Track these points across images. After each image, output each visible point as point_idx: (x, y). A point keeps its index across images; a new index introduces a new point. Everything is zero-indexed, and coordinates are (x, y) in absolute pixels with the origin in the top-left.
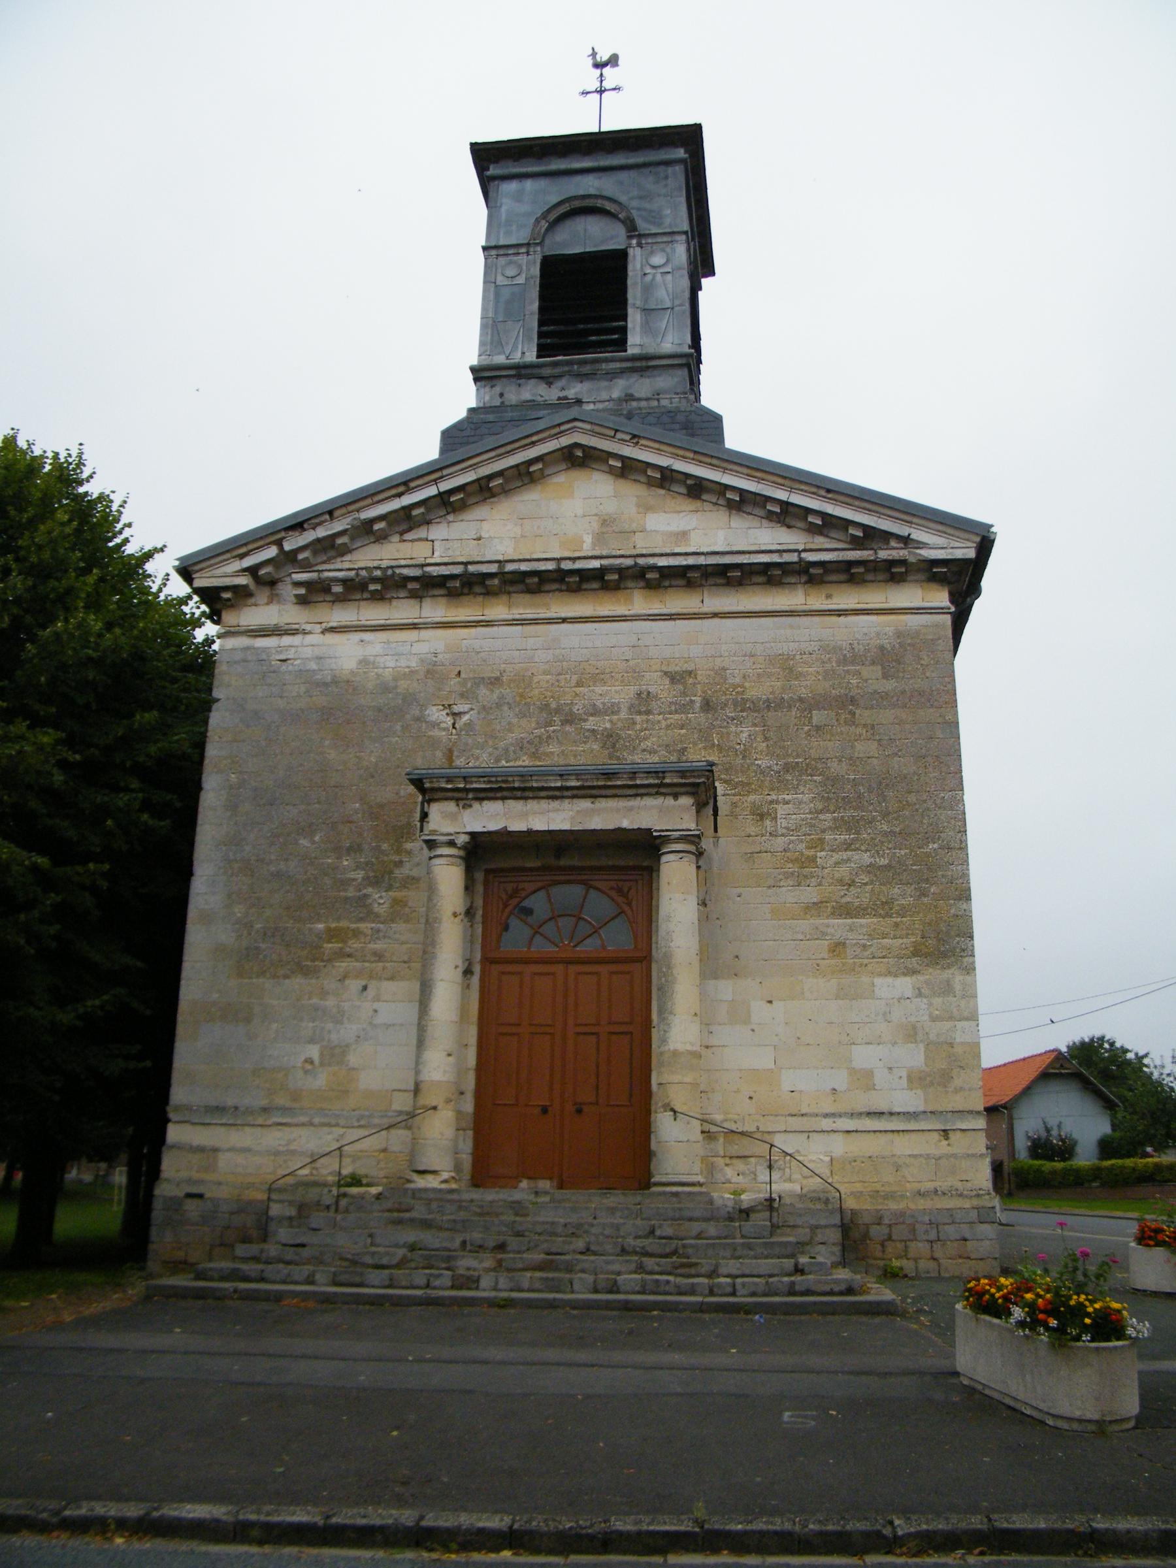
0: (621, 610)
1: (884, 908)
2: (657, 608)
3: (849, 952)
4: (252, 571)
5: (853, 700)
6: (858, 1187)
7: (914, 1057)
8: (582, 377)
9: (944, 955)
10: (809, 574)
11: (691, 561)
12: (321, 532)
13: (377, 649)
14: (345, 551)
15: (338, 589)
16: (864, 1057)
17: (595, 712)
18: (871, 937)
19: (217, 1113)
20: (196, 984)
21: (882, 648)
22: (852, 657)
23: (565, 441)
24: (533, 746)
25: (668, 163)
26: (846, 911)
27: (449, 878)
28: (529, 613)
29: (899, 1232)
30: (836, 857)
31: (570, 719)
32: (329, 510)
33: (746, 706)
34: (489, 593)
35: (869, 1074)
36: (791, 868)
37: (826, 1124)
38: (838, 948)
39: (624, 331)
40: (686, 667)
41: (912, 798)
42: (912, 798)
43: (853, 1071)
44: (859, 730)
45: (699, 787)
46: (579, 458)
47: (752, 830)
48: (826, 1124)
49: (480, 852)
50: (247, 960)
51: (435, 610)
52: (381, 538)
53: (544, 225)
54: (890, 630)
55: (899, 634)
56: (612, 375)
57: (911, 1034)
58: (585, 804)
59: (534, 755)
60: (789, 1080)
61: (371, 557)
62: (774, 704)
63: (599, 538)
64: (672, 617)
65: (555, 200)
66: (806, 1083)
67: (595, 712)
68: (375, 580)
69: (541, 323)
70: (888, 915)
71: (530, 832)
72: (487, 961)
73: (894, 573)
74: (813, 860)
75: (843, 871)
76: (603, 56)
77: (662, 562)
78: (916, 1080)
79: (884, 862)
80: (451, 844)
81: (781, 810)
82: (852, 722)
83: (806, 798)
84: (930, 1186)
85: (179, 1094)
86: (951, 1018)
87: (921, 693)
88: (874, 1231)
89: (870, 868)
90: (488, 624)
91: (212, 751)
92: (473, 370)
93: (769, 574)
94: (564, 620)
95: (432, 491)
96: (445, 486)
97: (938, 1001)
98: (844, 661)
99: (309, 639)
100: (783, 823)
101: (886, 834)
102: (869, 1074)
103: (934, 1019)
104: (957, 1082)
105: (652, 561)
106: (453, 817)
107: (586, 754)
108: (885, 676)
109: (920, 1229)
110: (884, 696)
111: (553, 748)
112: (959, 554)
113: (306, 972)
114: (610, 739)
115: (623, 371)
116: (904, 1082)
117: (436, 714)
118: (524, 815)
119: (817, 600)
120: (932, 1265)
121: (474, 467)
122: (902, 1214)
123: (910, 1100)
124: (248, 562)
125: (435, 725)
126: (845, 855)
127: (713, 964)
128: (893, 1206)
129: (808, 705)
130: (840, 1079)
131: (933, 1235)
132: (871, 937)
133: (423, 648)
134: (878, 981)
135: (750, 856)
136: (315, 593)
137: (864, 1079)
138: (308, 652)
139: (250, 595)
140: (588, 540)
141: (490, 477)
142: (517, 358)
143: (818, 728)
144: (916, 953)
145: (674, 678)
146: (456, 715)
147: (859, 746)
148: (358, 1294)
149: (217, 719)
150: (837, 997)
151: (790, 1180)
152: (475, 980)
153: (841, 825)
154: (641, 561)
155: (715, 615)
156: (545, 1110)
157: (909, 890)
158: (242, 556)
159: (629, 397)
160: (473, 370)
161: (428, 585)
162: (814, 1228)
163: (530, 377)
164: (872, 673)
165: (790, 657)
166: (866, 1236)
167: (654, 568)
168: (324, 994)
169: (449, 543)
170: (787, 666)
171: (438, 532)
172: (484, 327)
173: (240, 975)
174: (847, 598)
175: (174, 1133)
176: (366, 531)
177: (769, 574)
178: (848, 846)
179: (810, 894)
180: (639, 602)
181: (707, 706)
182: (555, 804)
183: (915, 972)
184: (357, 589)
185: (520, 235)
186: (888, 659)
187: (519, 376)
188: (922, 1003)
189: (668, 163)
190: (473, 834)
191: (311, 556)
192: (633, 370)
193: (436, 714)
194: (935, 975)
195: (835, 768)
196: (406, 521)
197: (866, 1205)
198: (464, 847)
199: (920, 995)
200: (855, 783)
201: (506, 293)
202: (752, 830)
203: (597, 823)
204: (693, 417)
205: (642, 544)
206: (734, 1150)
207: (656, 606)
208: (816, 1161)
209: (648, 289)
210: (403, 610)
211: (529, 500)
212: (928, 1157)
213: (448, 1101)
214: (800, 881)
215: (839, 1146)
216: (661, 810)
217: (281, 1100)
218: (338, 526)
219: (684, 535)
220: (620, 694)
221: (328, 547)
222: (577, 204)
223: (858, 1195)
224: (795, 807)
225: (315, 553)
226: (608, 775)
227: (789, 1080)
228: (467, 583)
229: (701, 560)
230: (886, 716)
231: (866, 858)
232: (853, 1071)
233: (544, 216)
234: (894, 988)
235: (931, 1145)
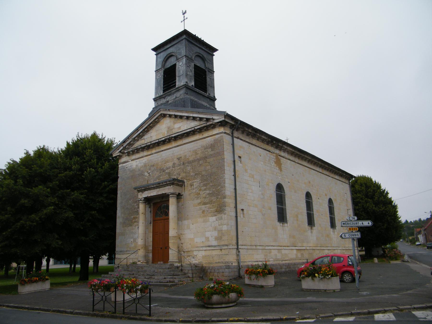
0: (171, 146)
1: (211, 202)
2: (176, 145)
3: (205, 212)
4: (120, 152)
5: (206, 157)
6: (206, 262)
7: (215, 234)
8: (169, 95)
9: (221, 211)
10: (200, 130)
11: (177, 134)
12: (128, 142)
13: (138, 163)
14: (133, 144)
15: (131, 152)
16: (208, 234)
17: (167, 169)
18: (209, 209)
19: (122, 252)
20: (118, 231)
21: (211, 144)
22: (206, 148)
23: (159, 114)
24: (158, 178)
25: (182, 40)
26: (205, 204)
27: (142, 206)
28: (157, 150)
29: (213, 271)
30: (203, 192)
31: (164, 171)
32: (128, 138)
33: (189, 162)
34: (153, 148)
35: (208, 238)
36: (196, 196)
37: (201, 249)
38: (203, 212)
39: (175, 82)
40: (180, 156)
41: (216, 177)
42: (216, 177)
43: (206, 238)
44: (207, 164)
45: (178, 183)
46: (164, 116)
47: (190, 189)
48: (201, 249)
49: (147, 200)
50: (124, 224)
51: (145, 153)
52: (138, 140)
53: (164, 62)
54: (213, 140)
55: (214, 140)
56: (174, 93)
57: (215, 229)
58: (158, 189)
59: (159, 180)
60: (196, 240)
61: (138, 144)
62: (194, 161)
63: (168, 132)
64: (178, 146)
65: (165, 56)
66: (199, 240)
67: (167, 169)
68: (135, 150)
69: (164, 85)
70: (212, 204)
71: (151, 196)
72: (154, 221)
73: (214, 126)
74: (199, 193)
75: (204, 195)
76: (184, 12)
77: (173, 136)
78: (217, 239)
79: (211, 192)
80: (141, 200)
81: (195, 184)
82: (206, 162)
83: (198, 180)
84: (218, 261)
85: (117, 249)
86: (222, 225)
87: (218, 153)
88: (209, 271)
89: (209, 194)
90: (152, 154)
91: (119, 187)
92: (154, 99)
93: (187, 134)
94: (162, 151)
95: (141, 130)
96: (144, 128)
97: (220, 221)
98: (205, 149)
99: (130, 163)
100: (195, 186)
101: (211, 186)
102: (208, 238)
103: (219, 225)
104: (223, 239)
105: (172, 136)
106: (141, 195)
107: (164, 178)
108: (212, 151)
109: (216, 270)
110: (211, 155)
111: (161, 177)
112: (221, 120)
113: (131, 225)
114: (169, 174)
115: (175, 92)
116: (214, 239)
117: (146, 174)
118: (158, 191)
119: (200, 136)
120: (218, 278)
121: (147, 123)
122: (213, 267)
123: (214, 243)
124: (119, 150)
125: (146, 176)
126: (204, 192)
127: (180, 218)
128: (211, 265)
129: (199, 160)
130: (204, 239)
131: (218, 271)
132: (209, 209)
133: (144, 161)
134: (210, 218)
135: (190, 194)
136: (129, 154)
137: (207, 239)
138: (130, 165)
139: (122, 156)
140: (166, 133)
141: (150, 124)
142: (160, 95)
143: (200, 165)
144: (216, 211)
145: (179, 159)
146: (149, 173)
147: (207, 167)
148: (270, 297)
149: (119, 180)
150: (203, 222)
151: (196, 260)
152: (152, 224)
153: (205, 185)
154: (170, 136)
155: (184, 144)
156: (161, 248)
157: (215, 197)
158: (118, 149)
159: (176, 97)
160: (154, 99)
161: (148, 147)
162: (188, 270)
163: (161, 98)
164: (209, 150)
165: (196, 150)
166: (207, 271)
167: (172, 137)
168: (133, 229)
169: (153, 136)
170: (195, 152)
171: (145, 137)
172: (155, 89)
173: (123, 227)
174: (206, 134)
175: (117, 256)
176: (135, 140)
177: (187, 134)
178: (205, 190)
179: (199, 201)
180: (174, 144)
181: (183, 164)
182: (154, 190)
183: (216, 215)
184: (137, 150)
185: (160, 67)
186: (212, 146)
187: (160, 98)
188: (217, 222)
189: (182, 40)
190: (145, 198)
191: (134, 143)
192: (177, 91)
193: (146, 174)
194: (219, 216)
195: (203, 173)
196: (140, 136)
197: (207, 265)
198: (144, 200)
199: (217, 220)
200: (206, 176)
201: (159, 80)
202: (190, 189)
203: (160, 193)
204: (185, 99)
205: (175, 131)
206: (188, 255)
207: (149, 153)
208: (199, 257)
209: (179, 71)
210: (141, 154)
211: (158, 126)
212: (218, 255)
213: (142, 248)
214: (197, 198)
215: (204, 253)
216: (169, 189)
217: (129, 249)
218: (130, 140)
219: (180, 128)
220: (170, 164)
221: (129, 144)
222: (168, 56)
223: (206, 263)
224: (197, 183)
225: (129, 146)
226: (159, 184)
227: (196, 240)
228: (148, 147)
229: (179, 134)
230: (212, 159)
231: (208, 192)
232: (206, 238)
233: (164, 60)
234: (212, 219)
235: (217, 252)
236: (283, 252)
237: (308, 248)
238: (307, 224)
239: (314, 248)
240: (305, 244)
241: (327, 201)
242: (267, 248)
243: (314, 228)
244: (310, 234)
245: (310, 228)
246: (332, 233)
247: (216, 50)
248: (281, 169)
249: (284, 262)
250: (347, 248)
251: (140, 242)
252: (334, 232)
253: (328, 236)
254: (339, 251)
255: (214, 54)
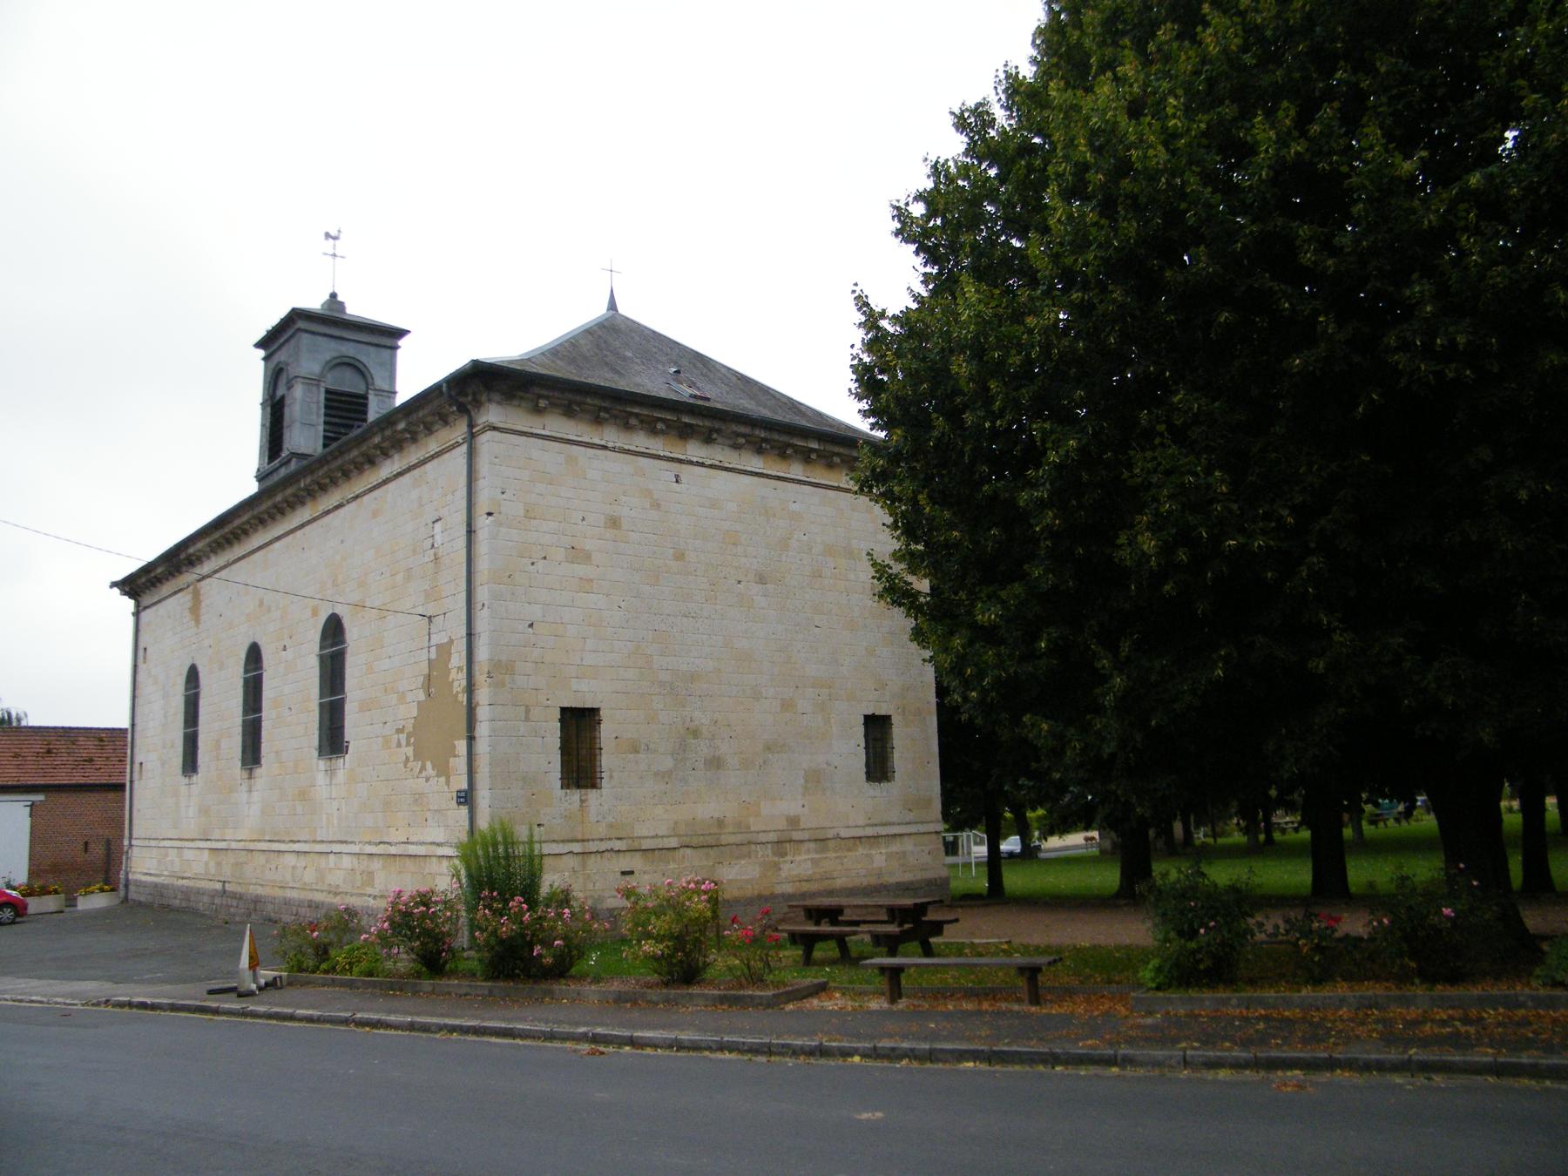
172: (820, 414)
236: (189, 854)
237: (234, 845)
238: (239, 764)
239: (251, 846)
240: (229, 834)
241: (243, 655)
242: (163, 843)
243: (258, 772)
244: (244, 796)
245: (245, 774)
246: (321, 779)
247: (400, 333)
248: (197, 621)
249: (181, 882)
250: (393, 850)
251: (1272, 993)
252: (331, 772)
253: (304, 795)
254: (347, 862)
255: (400, 343)
